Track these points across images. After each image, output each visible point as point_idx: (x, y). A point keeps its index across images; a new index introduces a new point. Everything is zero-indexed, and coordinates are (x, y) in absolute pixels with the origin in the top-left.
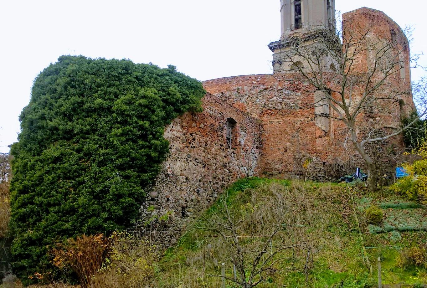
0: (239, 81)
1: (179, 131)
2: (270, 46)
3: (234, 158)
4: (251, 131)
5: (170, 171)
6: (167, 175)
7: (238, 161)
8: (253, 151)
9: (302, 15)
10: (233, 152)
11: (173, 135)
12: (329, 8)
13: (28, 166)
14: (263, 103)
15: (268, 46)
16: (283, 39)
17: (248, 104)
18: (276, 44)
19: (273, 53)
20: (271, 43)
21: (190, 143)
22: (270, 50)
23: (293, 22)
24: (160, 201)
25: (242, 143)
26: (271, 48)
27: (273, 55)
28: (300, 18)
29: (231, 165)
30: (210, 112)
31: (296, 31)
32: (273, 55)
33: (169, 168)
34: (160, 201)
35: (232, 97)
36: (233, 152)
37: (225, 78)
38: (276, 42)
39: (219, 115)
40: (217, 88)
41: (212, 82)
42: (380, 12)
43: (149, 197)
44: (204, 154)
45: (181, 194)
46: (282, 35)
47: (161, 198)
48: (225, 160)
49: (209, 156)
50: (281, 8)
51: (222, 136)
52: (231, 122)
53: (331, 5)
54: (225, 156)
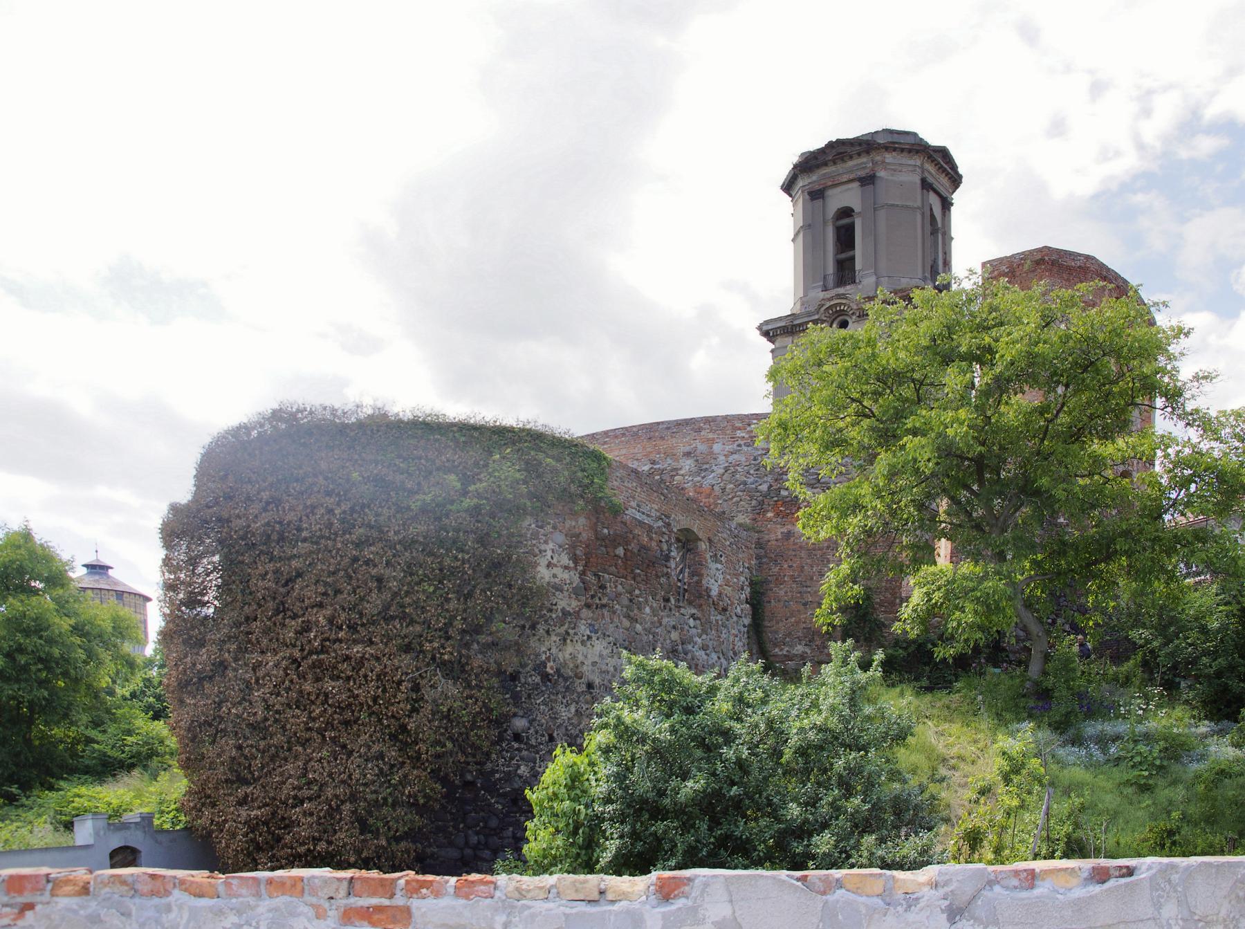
0: (699, 430)
1: (566, 568)
2: (765, 328)
3: (694, 631)
4: (734, 559)
5: (552, 668)
6: (546, 677)
7: (704, 637)
8: (739, 610)
9: (858, 252)
10: (692, 616)
11: (555, 576)
12: (934, 231)
13: (1100, 727)
14: (764, 488)
15: (760, 328)
16: (797, 311)
17: (723, 490)
18: (783, 324)
19: (772, 346)
20: (767, 322)
21: (593, 597)
22: (764, 340)
23: (831, 268)
24: (533, 742)
25: (714, 593)
26: (766, 334)
27: (772, 351)
28: (853, 258)
29: (690, 647)
30: (638, 516)
31: (841, 290)
32: (772, 351)
33: (548, 659)
34: (533, 742)
35: (681, 472)
36: (692, 616)
37: (658, 423)
38: (780, 319)
39: (660, 523)
40: (638, 449)
41: (623, 435)
42: (1088, 257)
43: (509, 732)
44: (626, 623)
45: (580, 723)
46: (804, 301)
47: (537, 732)
48: (675, 635)
49: (639, 627)
50: (796, 235)
51: (668, 575)
52: (687, 541)
53: (940, 225)
54: (674, 627)
